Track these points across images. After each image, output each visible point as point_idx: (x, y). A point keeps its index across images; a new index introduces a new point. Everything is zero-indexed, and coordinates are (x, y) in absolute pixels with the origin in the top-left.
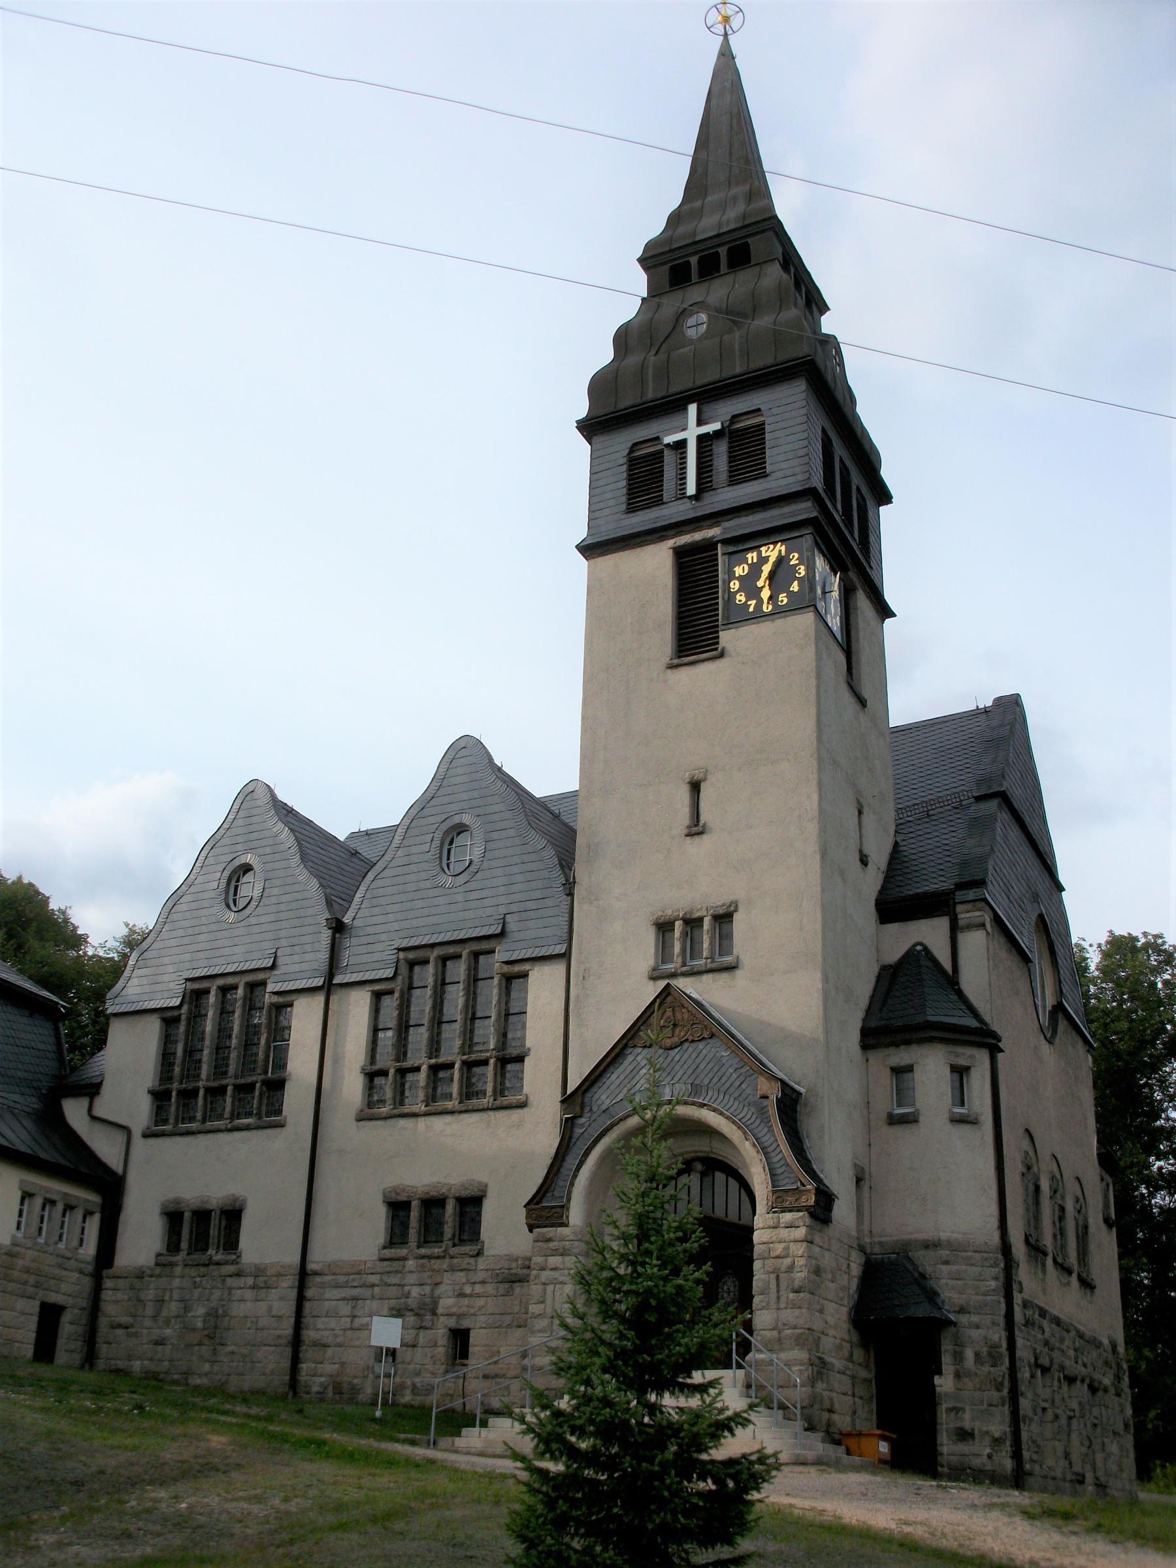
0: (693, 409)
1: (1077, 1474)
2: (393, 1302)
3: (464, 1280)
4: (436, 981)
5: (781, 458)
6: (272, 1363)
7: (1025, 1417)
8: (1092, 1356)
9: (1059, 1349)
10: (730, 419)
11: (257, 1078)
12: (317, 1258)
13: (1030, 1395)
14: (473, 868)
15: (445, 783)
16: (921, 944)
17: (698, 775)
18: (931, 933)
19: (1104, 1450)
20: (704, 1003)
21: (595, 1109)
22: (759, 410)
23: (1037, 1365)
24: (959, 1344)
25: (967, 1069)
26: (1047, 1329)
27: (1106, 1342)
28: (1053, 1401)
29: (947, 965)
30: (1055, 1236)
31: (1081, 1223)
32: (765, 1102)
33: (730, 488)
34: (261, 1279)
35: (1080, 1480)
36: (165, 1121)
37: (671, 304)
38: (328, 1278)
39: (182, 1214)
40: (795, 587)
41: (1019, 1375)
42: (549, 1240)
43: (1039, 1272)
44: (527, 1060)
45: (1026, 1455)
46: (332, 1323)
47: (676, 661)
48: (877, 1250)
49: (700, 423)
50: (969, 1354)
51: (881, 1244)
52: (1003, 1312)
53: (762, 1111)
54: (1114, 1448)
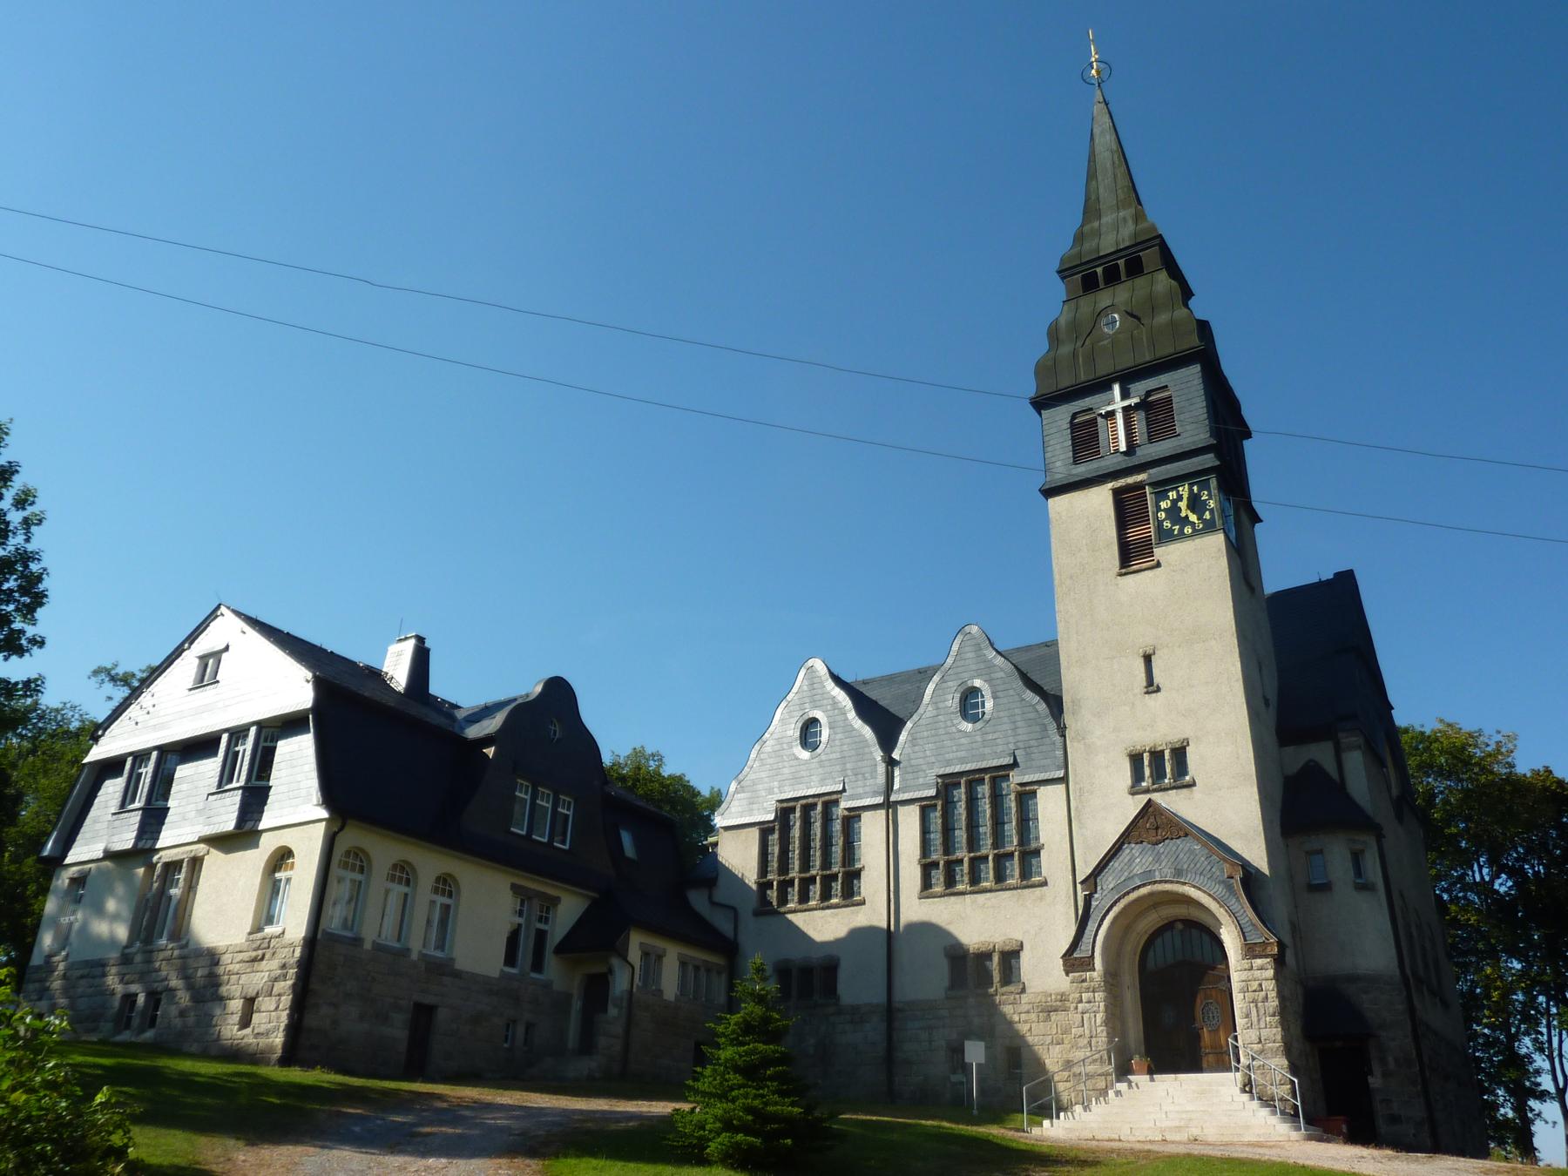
0: (1117, 388)
12: (898, 997)
17: (1149, 651)
18: (1321, 753)
25: (1362, 851)
29: (1334, 774)
34: (857, 1015)
37: (1086, 304)
50: (1390, 1059)
53: (1230, 888)
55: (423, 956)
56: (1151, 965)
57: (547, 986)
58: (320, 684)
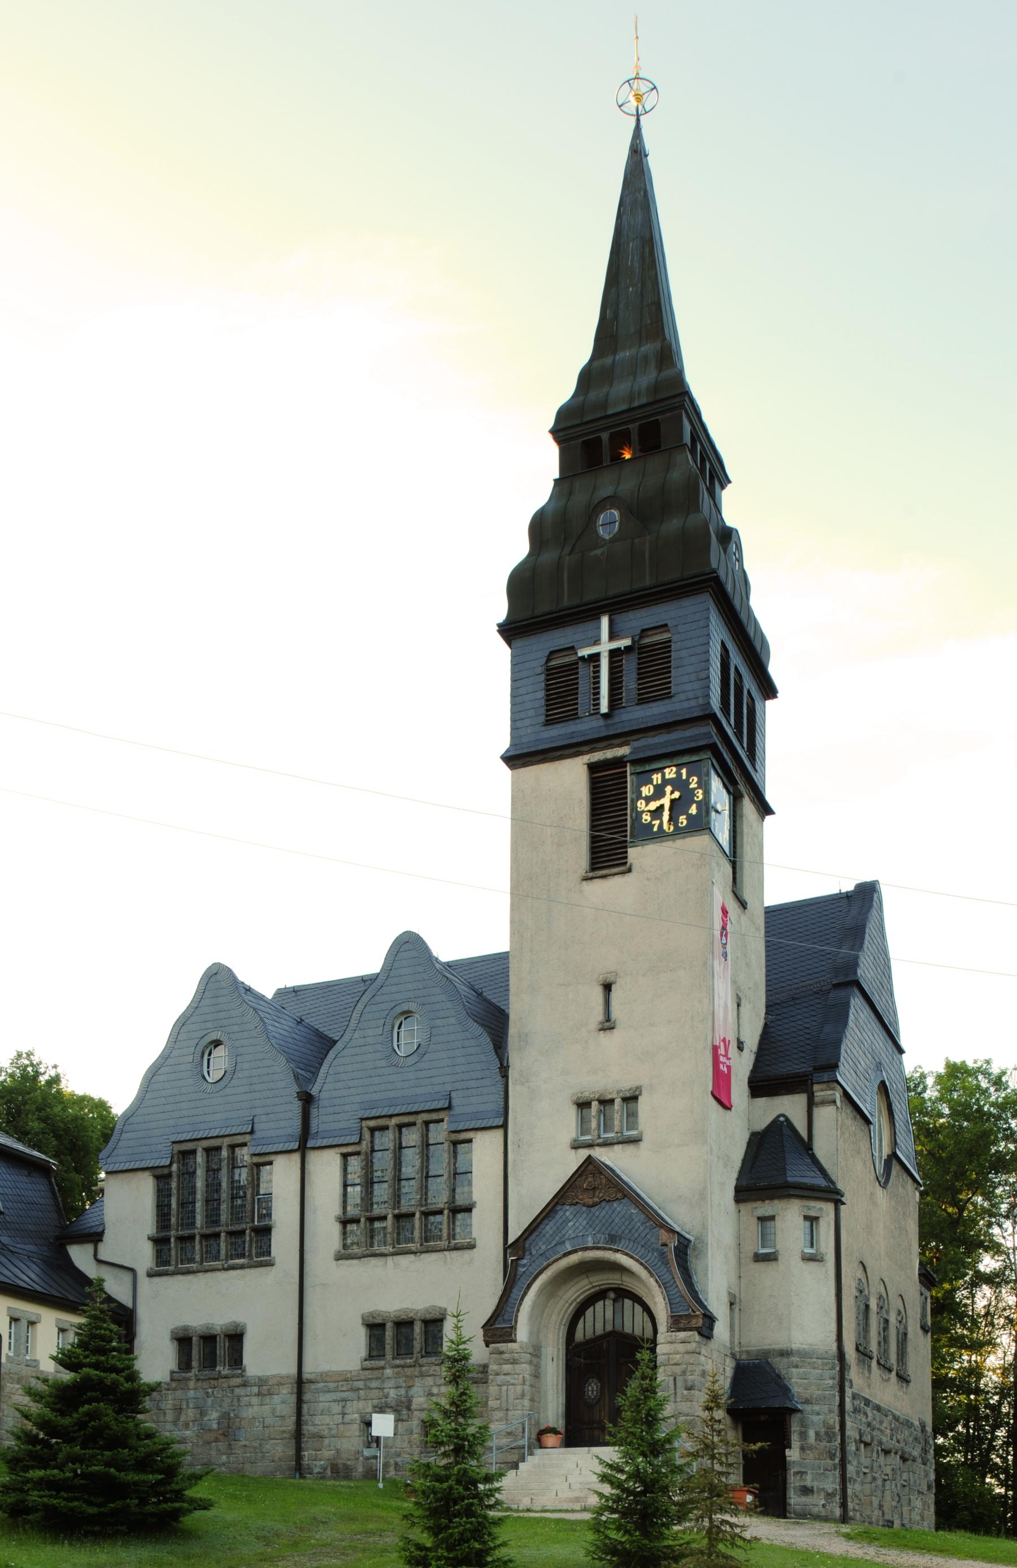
0: (605, 621)
1: (889, 1521)
2: (375, 1402)
3: (432, 1383)
4: (450, 1171)
5: (685, 679)
6: (280, 1450)
7: (850, 1478)
8: (905, 1434)
9: (878, 1429)
10: (630, 609)
11: (246, 1226)
12: (310, 1368)
13: (855, 1463)
14: (421, 1050)
15: (392, 974)
16: (783, 1115)
17: (610, 978)
18: (791, 1107)
19: (909, 1504)
20: (615, 1168)
21: (534, 1252)
22: (666, 625)
23: (861, 1441)
24: (804, 1424)
25: (817, 1219)
26: (870, 1414)
27: (917, 1423)
28: (872, 1468)
29: (804, 1133)
30: (879, 1343)
31: (901, 1331)
32: (665, 1249)
33: (638, 707)
34: (264, 1387)
35: (890, 1524)
36: (167, 1263)
38: (321, 1385)
39: (190, 1339)
40: (693, 810)
41: (848, 1448)
42: (502, 1353)
43: (866, 1372)
44: (474, 1211)
45: (850, 1506)
46: (327, 1419)
47: (590, 875)
48: (744, 1356)
49: (612, 637)
50: (812, 1434)
51: (748, 1352)
52: (837, 1403)
53: (662, 1255)
54: (918, 1503)
56: (579, 1336)
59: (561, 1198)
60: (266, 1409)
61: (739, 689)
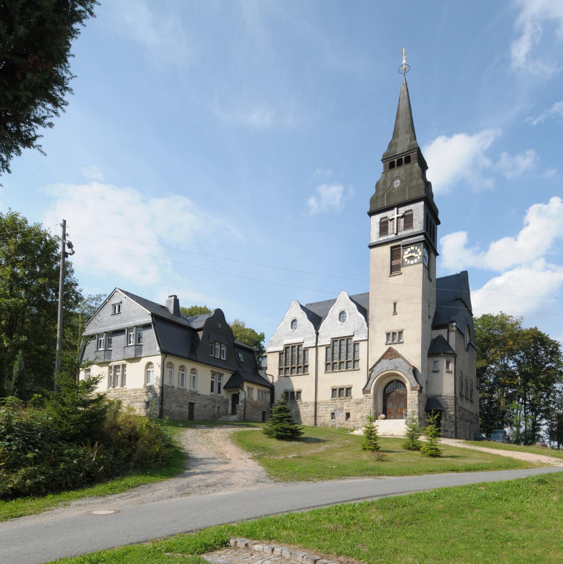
12: (319, 400)
18: (443, 332)
29: (446, 339)
53: (409, 372)
55: (190, 390)
57: (222, 397)
58: (153, 315)
59: (383, 357)
60: (307, 410)
61: (431, 223)
